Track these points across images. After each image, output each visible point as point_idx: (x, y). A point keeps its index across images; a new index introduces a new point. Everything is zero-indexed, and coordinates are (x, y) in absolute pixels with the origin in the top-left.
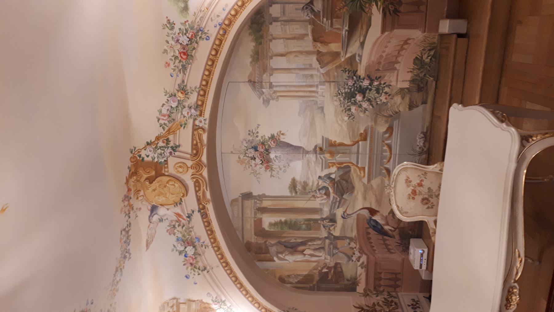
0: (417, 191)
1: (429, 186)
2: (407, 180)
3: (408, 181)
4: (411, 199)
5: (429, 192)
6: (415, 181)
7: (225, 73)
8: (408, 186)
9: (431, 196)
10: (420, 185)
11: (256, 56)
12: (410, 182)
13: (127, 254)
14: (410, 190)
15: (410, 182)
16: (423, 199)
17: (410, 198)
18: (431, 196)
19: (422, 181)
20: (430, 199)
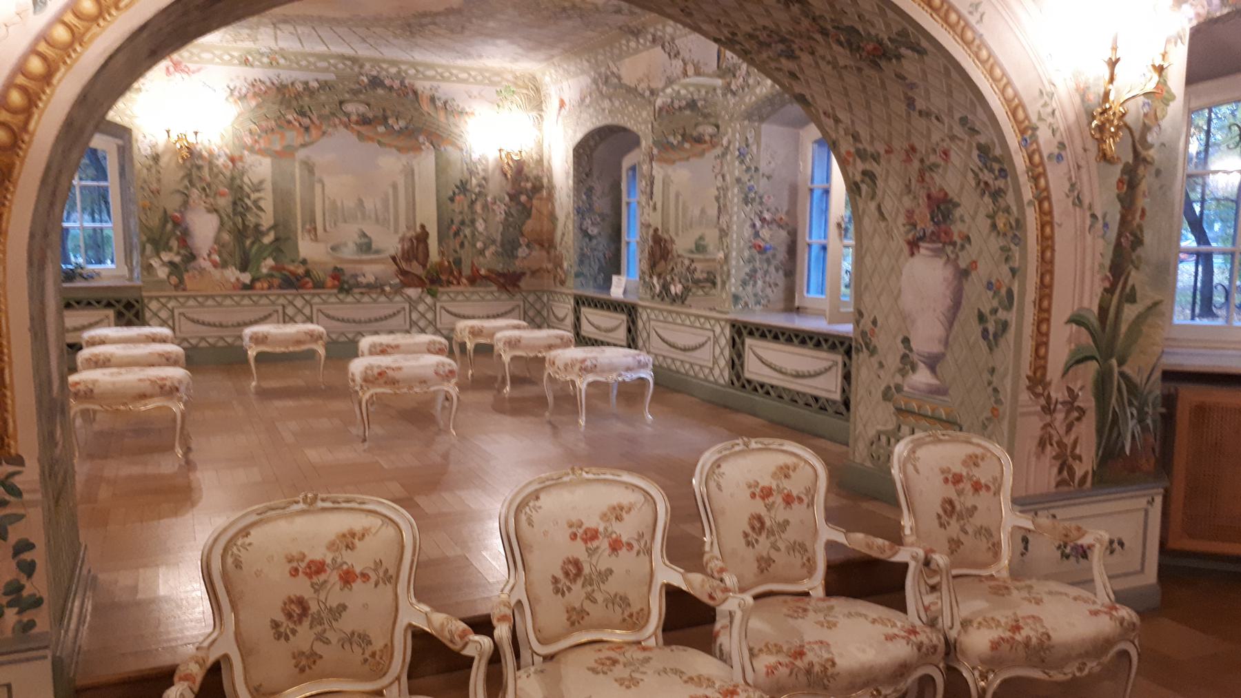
0: (595, 543)
1: (979, 507)
2: (622, 509)
3: (618, 512)
4: (288, 567)
5: (967, 509)
6: (625, 530)
7: (32, 329)
8: (604, 516)
9: (960, 517)
10: (616, 546)
11: (379, 349)
12: (976, 465)
13: (1098, 136)
14: (593, 522)
15: (976, 465)
16: (301, 603)
17: (290, 561)
18: (960, 517)
19: (988, 488)
20: (580, 582)
